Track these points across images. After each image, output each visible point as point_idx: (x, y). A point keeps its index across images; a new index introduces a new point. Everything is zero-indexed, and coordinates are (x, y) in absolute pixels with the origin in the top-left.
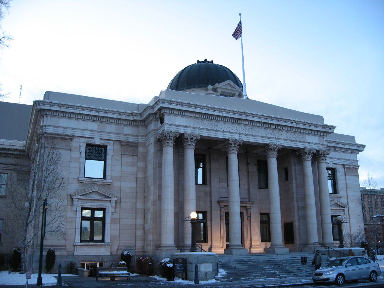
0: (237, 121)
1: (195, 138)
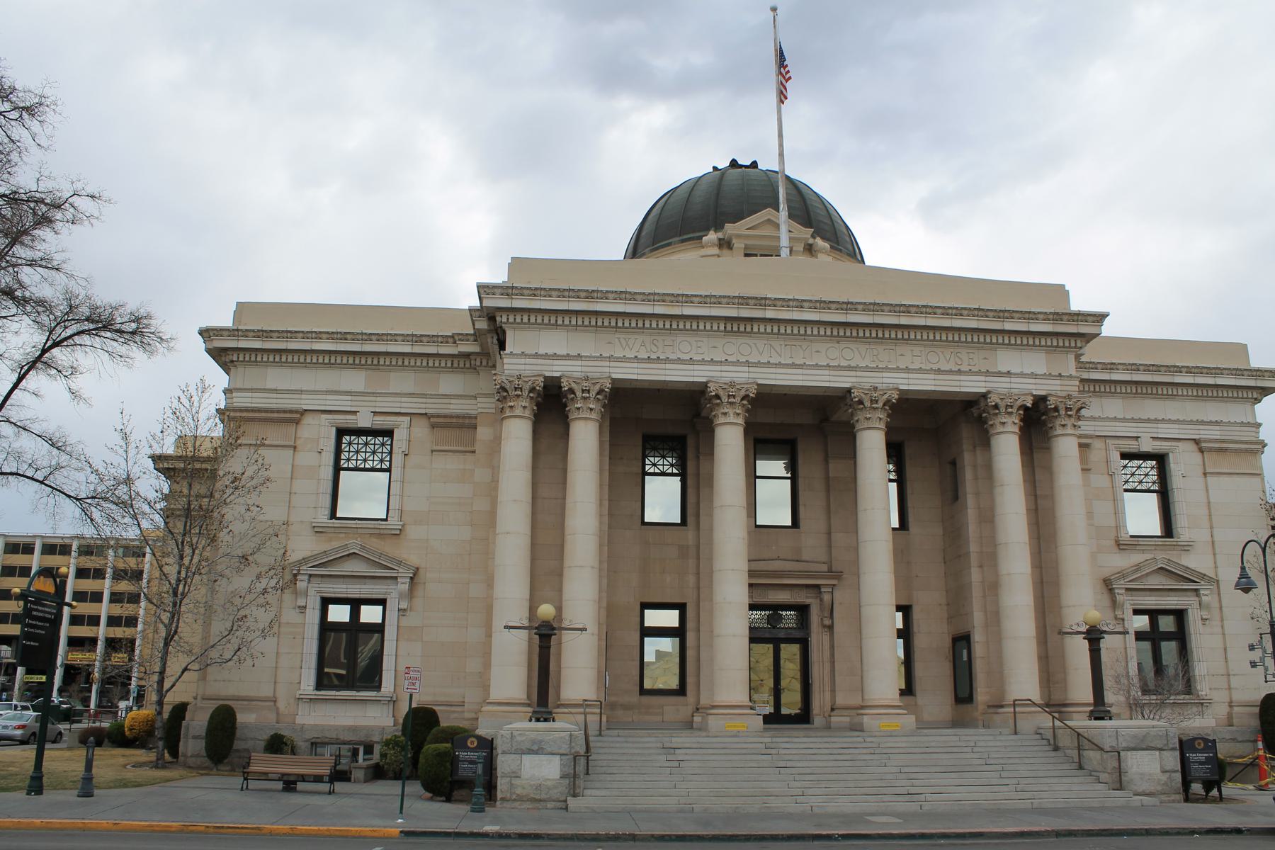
0: (736, 326)
1: (597, 387)
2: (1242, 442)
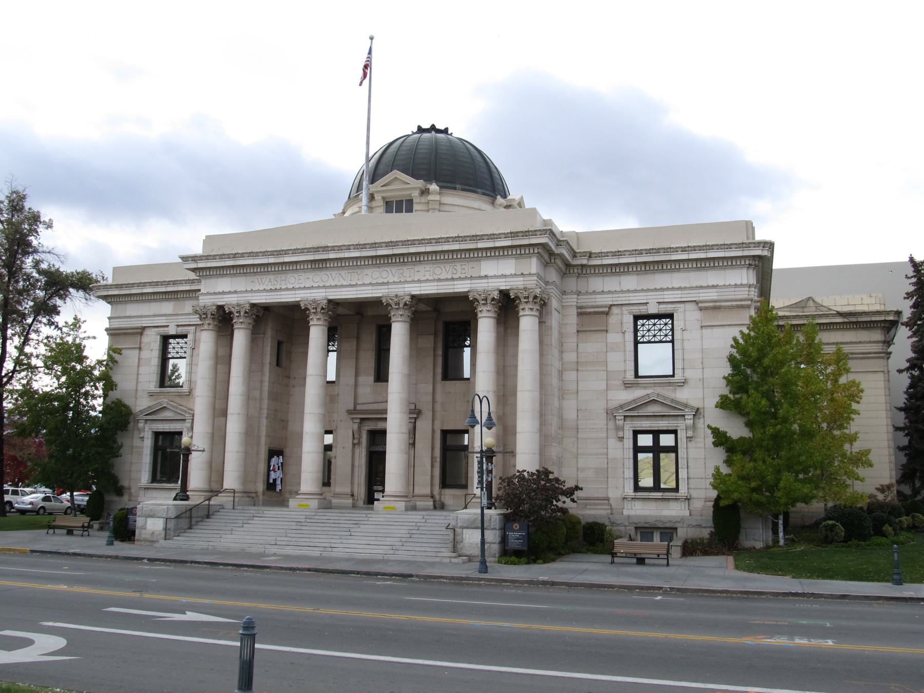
0: (318, 265)
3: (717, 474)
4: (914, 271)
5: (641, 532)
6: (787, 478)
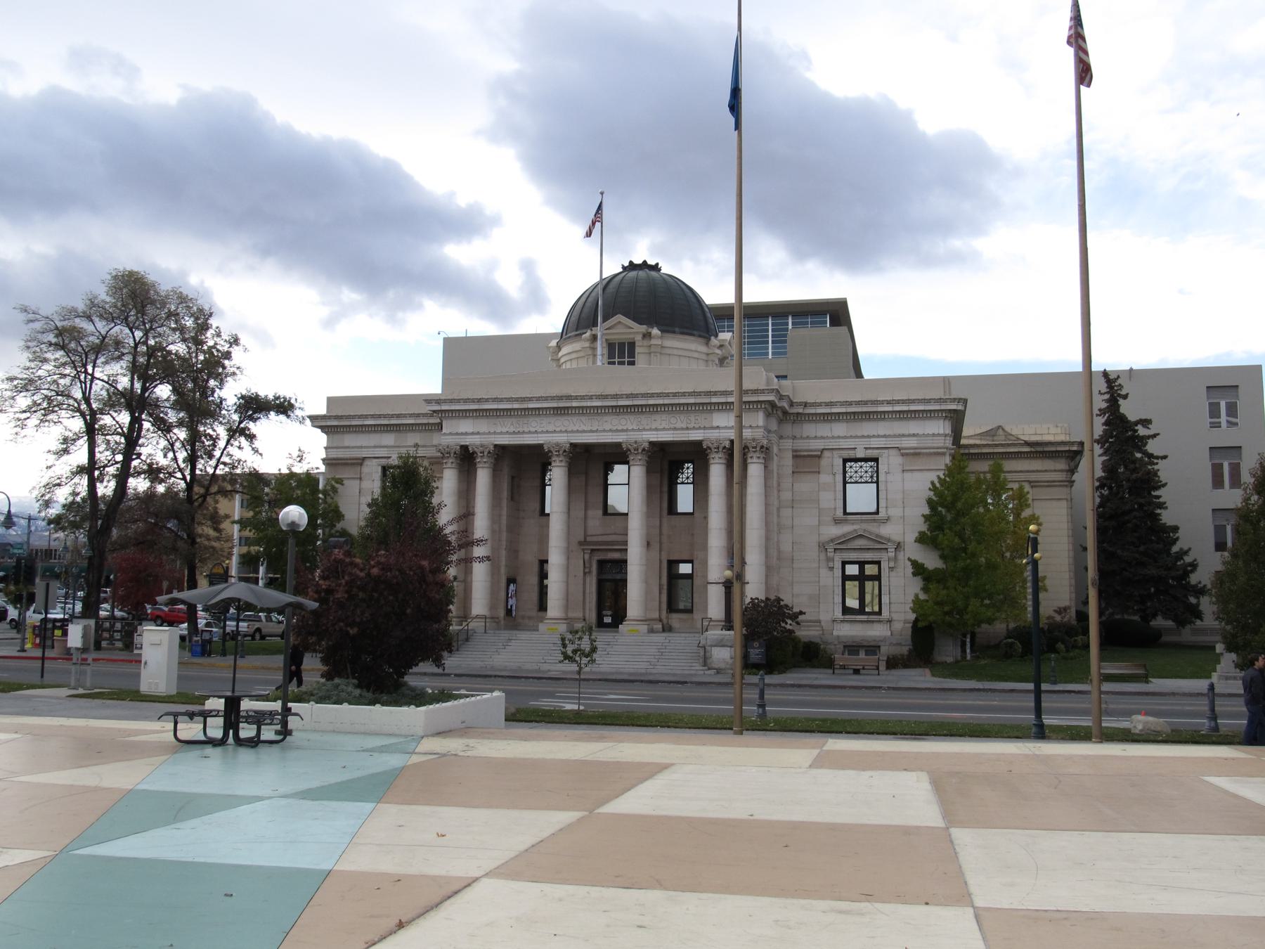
1: (487, 450)
2: (934, 448)
3: (916, 601)
4: (1107, 387)
5: (849, 651)
6: (974, 604)
